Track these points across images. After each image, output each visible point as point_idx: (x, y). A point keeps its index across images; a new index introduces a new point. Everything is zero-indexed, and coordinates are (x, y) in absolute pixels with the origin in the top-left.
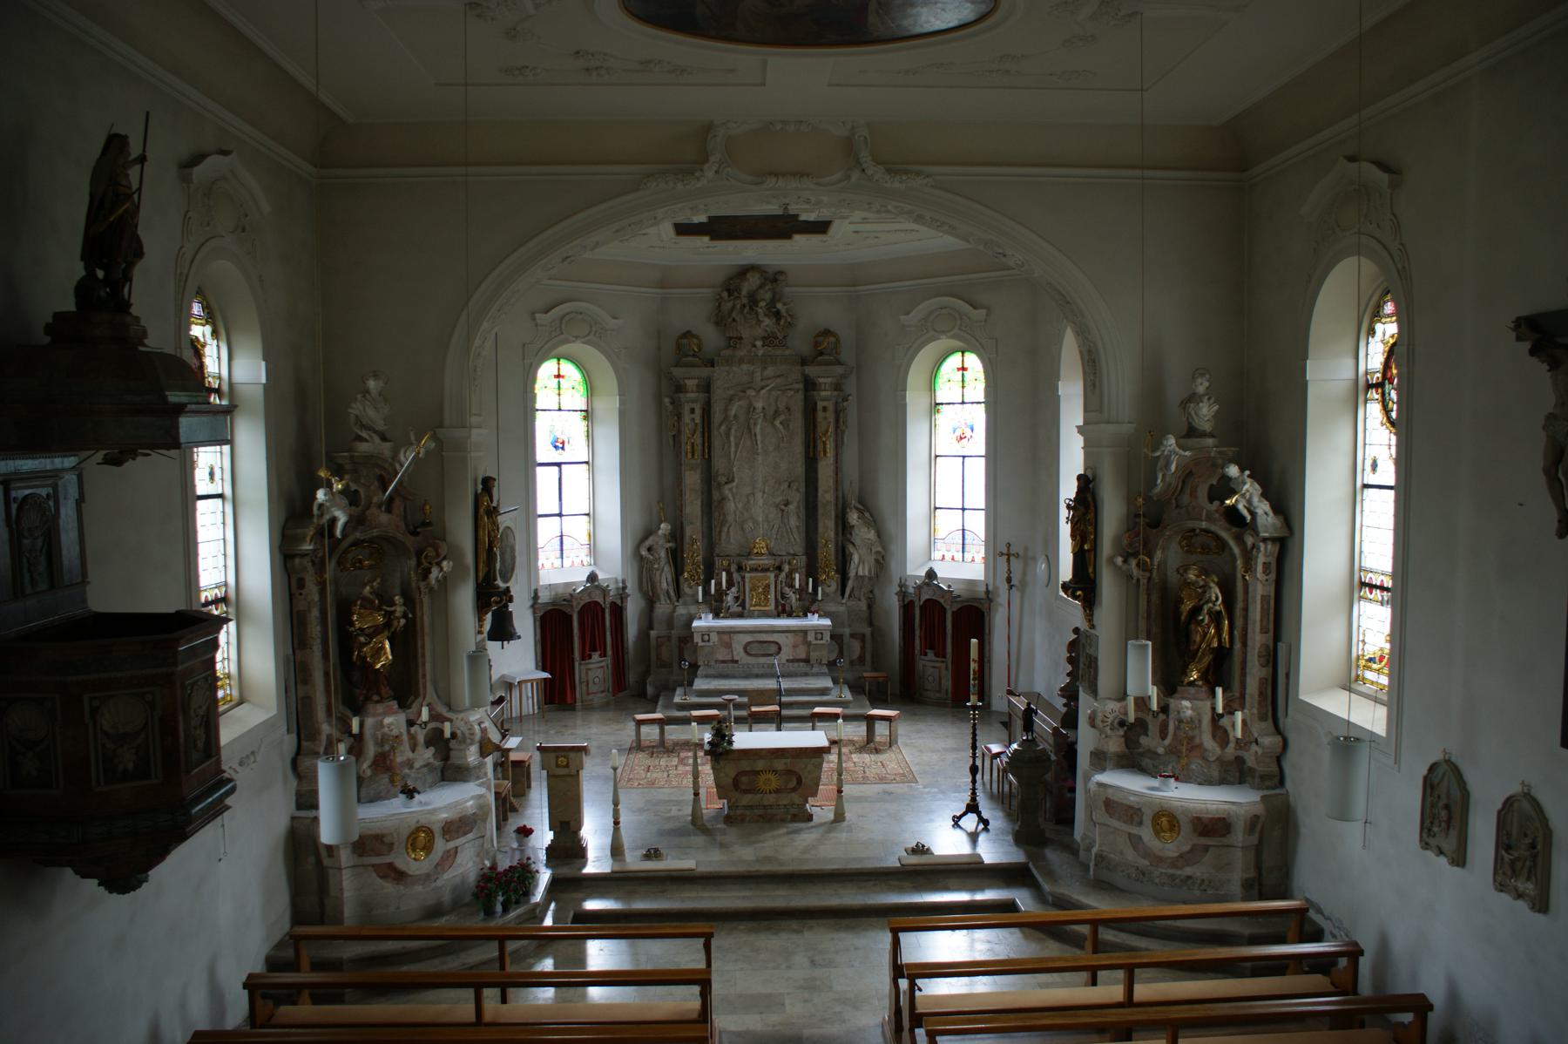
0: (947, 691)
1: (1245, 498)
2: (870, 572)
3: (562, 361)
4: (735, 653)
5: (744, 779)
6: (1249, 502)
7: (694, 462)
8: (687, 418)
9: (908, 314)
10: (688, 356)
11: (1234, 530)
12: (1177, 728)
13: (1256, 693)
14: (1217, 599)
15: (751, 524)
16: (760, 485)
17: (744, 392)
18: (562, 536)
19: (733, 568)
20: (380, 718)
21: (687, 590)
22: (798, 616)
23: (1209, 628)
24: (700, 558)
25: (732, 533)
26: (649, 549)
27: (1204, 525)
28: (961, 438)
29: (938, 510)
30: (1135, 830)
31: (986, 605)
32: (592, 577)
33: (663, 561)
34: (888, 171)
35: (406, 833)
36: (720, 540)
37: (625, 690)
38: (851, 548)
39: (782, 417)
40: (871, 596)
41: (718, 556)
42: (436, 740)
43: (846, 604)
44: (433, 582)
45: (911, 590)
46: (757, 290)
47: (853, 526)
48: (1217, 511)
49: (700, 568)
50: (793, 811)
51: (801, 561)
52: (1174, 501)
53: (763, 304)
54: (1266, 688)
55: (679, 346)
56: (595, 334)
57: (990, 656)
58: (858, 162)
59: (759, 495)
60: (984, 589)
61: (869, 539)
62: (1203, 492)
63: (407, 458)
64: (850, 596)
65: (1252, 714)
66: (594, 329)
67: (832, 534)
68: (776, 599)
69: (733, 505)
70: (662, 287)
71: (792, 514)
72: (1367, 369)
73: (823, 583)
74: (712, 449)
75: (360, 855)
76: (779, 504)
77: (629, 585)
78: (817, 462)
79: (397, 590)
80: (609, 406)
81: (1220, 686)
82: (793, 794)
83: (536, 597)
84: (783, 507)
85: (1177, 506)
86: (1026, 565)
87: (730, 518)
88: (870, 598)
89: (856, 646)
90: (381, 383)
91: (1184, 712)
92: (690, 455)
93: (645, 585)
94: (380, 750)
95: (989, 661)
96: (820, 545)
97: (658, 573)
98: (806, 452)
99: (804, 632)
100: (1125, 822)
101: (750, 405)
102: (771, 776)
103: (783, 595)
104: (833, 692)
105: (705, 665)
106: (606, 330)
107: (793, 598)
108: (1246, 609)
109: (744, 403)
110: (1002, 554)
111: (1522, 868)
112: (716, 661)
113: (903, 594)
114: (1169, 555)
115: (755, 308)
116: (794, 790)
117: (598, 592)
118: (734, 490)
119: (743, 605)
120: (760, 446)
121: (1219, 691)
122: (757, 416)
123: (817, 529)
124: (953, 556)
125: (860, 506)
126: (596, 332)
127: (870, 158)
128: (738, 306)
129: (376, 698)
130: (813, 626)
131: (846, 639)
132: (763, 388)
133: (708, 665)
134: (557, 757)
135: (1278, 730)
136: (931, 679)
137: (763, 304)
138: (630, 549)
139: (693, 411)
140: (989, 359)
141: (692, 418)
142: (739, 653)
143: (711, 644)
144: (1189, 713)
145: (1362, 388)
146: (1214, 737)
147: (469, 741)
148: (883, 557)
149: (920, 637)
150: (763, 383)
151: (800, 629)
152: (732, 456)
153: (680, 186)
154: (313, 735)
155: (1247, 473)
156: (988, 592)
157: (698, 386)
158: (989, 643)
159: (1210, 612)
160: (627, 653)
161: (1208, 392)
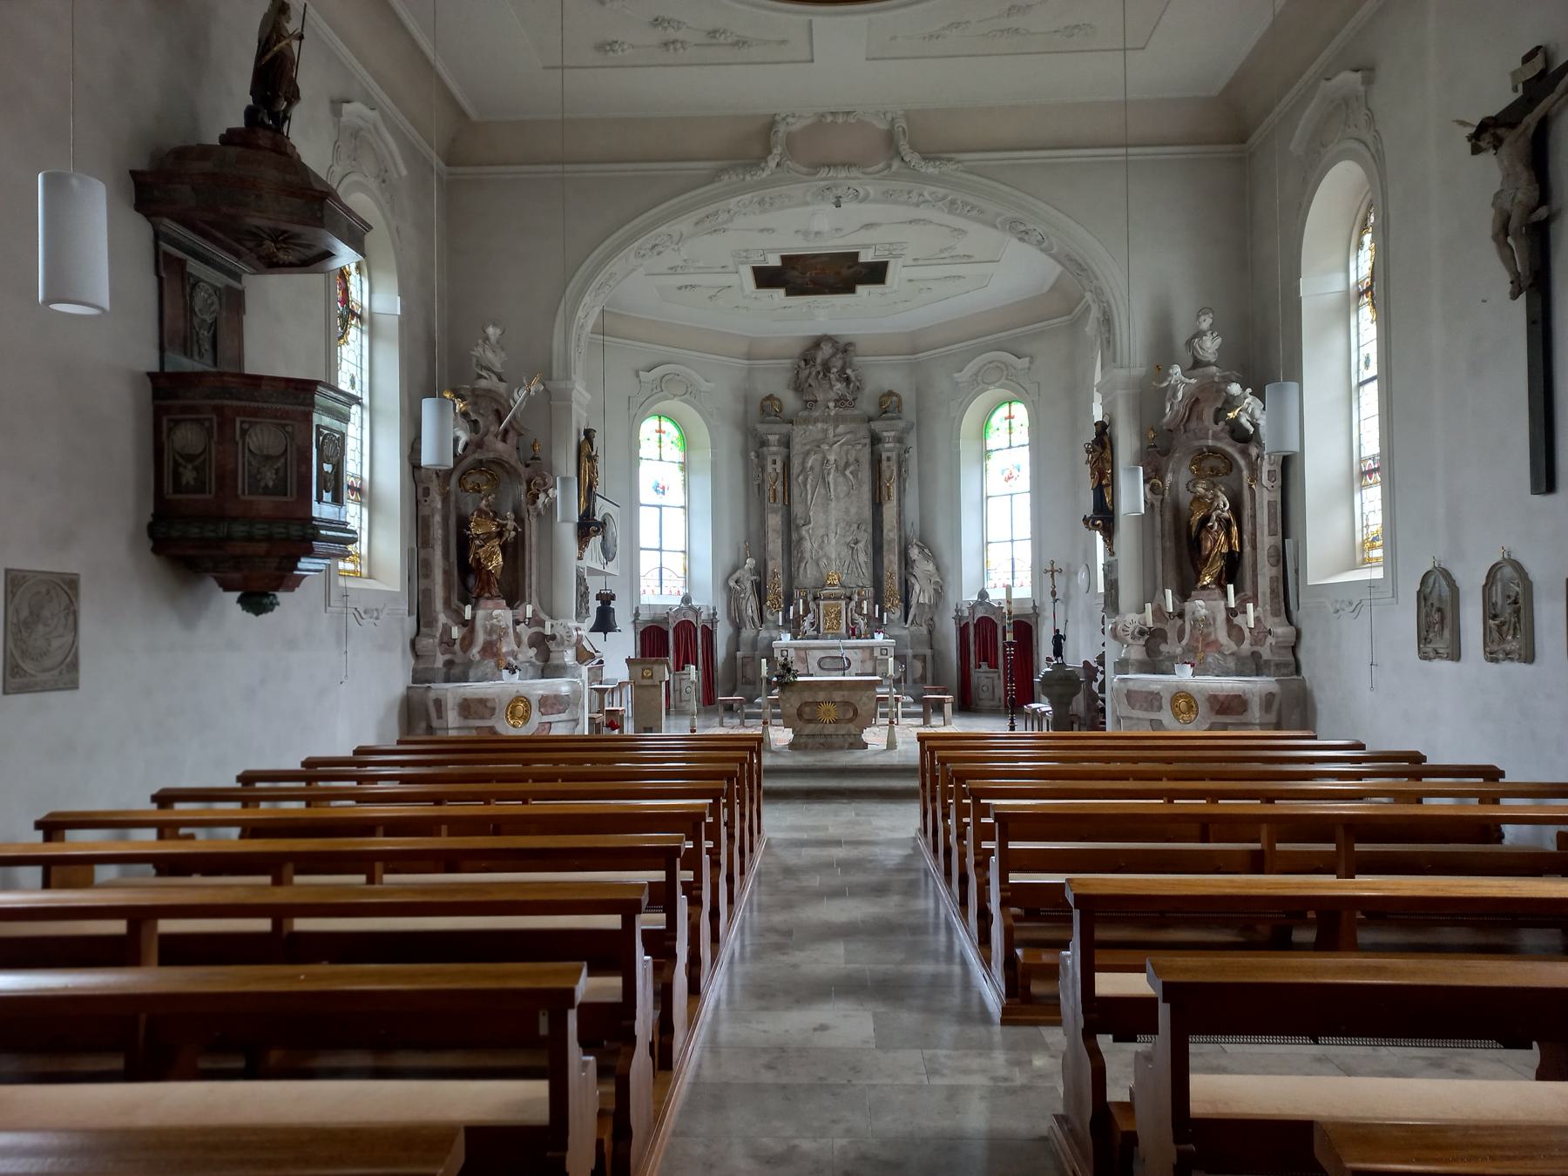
0: (1000, 699)
1: (1247, 413)
2: (930, 600)
5: (807, 709)
6: (1252, 415)
7: (775, 505)
8: (770, 468)
9: (960, 371)
10: (770, 415)
11: (1240, 445)
12: (1193, 627)
13: (1268, 591)
14: (1225, 506)
16: (833, 527)
17: (819, 447)
18: (661, 568)
19: (810, 598)
20: (489, 611)
21: (769, 617)
23: (1219, 535)
27: (1210, 443)
28: (1009, 478)
30: (1154, 716)
31: (1034, 620)
32: (686, 599)
33: (749, 591)
34: (924, 159)
35: (506, 701)
36: (798, 574)
39: (852, 468)
41: (797, 588)
42: (542, 643)
43: (908, 628)
44: (540, 506)
45: (966, 614)
46: (829, 358)
48: (1222, 430)
50: (850, 740)
51: (869, 592)
52: (1182, 427)
53: (834, 370)
54: (1277, 587)
55: (763, 409)
56: (690, 394)
57: (1038, 664)
58: (898, 153)
59: (832, 535)
62: (1208, 415)
63: (520, 396)
65: (1265, 611)
66: (690, 390)
67: (896, 568)
69: (809, 544)
70: (748, 359)
72: (1357, 280)
73: (888, 610)
75: (466, 718)
78: (882, 506)
79: (510, 505)
80: (704, 456)
81: (1231, 583)
83: (637, 615)
84: (853, 545)
85: (1185, 431)
86: (1069, 579)
87: (807, 555)
89: (918, 665)
90: (498, 332)
91: (1199, 611)
94: (488, 638)
96: (885, 578)
99: (871, 648)
100: (1145, 710)
101: (824, 457)
102: (830, 706)
106: (700, 392)
107: (862, 623)
108: (1254, 516)
109: (819, 456)
111: (1509, 629)
113: (958, 618)
114: (1179, 476)
116: (851, 720)
117: (691, 613)
119: (818, 630)
121: (1231, 588)
125: (920, 544)
126: (691, 392)
127: (908, 146)
128: (814, 373)
129: (487, 595)
131: (909, 660)
134: (643, 670)
135: (1290, 622)
137: (834, 370)
138: (720, 582)
139: (774, 462)
140: (1033, 401)
141: (774, 468)
144: (1203, 612)
145: (1349, 302)
146: (1229, 636)
147: (566, 643)
150: (836, 439)
152: (809, 503)
153: (748, 178)
154: (431, 623)
155: (1249, 390)
156: (1034, 607)
157: (779, 440)
159: (1219, 519)
161: (1212, 328)
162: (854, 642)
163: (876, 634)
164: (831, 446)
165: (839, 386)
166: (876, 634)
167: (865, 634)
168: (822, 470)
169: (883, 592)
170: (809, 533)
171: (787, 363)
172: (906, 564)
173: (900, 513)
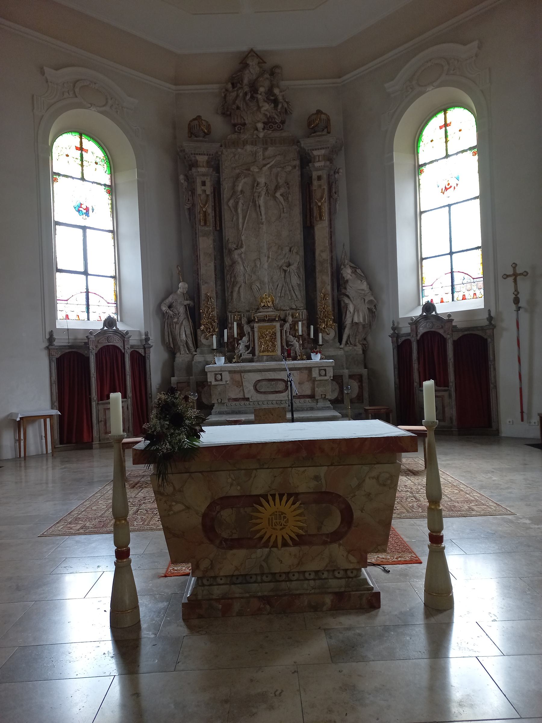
0: (451, 419)
2: (364, 320)
5: (227, 515)
7: (207, 229)
8: (199, 190)
15: (258, 285)
17: (248, 169)
19: (244, 321)
21: (204, 341)
22: (302, 359)
24: (215, 313)
25: (242, 294)
26: (170, 307)
28: (446, 189)
29: (424, 261)
36: (232, 299)
38: (347, 300)
39: (282, 190)
40: (365, 343)
41: (231, 312)
47: (347, 281)
49: (215, 322)
50: (335, 584)
51: (303, 313)
57: (496, 382)
60: (487, 316)
61: (363, 290)
64: (347, 343)
67: (329, 288)
68: (282, 346)
69: (242, 268)
70: (176, 84)
73: (323, 331)
77: (152, 337)
78: (314, 229)
82: (335, 546)
83: (51, 340)
84: (285, 268)
87: (240, 279)
88: (363, 344)
89: (355, 385)
92: (202, 223)
93: (167, 337)
95: (495, 387)
96: (319, 299)
97: (177, 326)
99: (309, 369)
101: (254, 180)
103: (287, 342)
107: (297, 345)
110: (508, 276)
112: (229, 399)
113: (396, 335)
115: (255, 95)
118: (243, 255)
119: (253, 353)
122: (260, 190)
123: (315, 283)
124: (442, 299)
128: (241, 95)
130: (317, 363)
131: (346, 379)
132: (265, 165)
133: (221, 403)
139: (204, 184)
142: (249, 391)
148: (375, 306)
149: (418, 370)
150: (265, 162)
152: (240, 226)
156: (490, 318)
157: (208, 162)
158: (495, 369)
160: (151, 398)
162: (290, 363)
164: (261, 169)
165: (266, 107)
167: (301, 356)
172: (339, 286)
173: (331, 234)
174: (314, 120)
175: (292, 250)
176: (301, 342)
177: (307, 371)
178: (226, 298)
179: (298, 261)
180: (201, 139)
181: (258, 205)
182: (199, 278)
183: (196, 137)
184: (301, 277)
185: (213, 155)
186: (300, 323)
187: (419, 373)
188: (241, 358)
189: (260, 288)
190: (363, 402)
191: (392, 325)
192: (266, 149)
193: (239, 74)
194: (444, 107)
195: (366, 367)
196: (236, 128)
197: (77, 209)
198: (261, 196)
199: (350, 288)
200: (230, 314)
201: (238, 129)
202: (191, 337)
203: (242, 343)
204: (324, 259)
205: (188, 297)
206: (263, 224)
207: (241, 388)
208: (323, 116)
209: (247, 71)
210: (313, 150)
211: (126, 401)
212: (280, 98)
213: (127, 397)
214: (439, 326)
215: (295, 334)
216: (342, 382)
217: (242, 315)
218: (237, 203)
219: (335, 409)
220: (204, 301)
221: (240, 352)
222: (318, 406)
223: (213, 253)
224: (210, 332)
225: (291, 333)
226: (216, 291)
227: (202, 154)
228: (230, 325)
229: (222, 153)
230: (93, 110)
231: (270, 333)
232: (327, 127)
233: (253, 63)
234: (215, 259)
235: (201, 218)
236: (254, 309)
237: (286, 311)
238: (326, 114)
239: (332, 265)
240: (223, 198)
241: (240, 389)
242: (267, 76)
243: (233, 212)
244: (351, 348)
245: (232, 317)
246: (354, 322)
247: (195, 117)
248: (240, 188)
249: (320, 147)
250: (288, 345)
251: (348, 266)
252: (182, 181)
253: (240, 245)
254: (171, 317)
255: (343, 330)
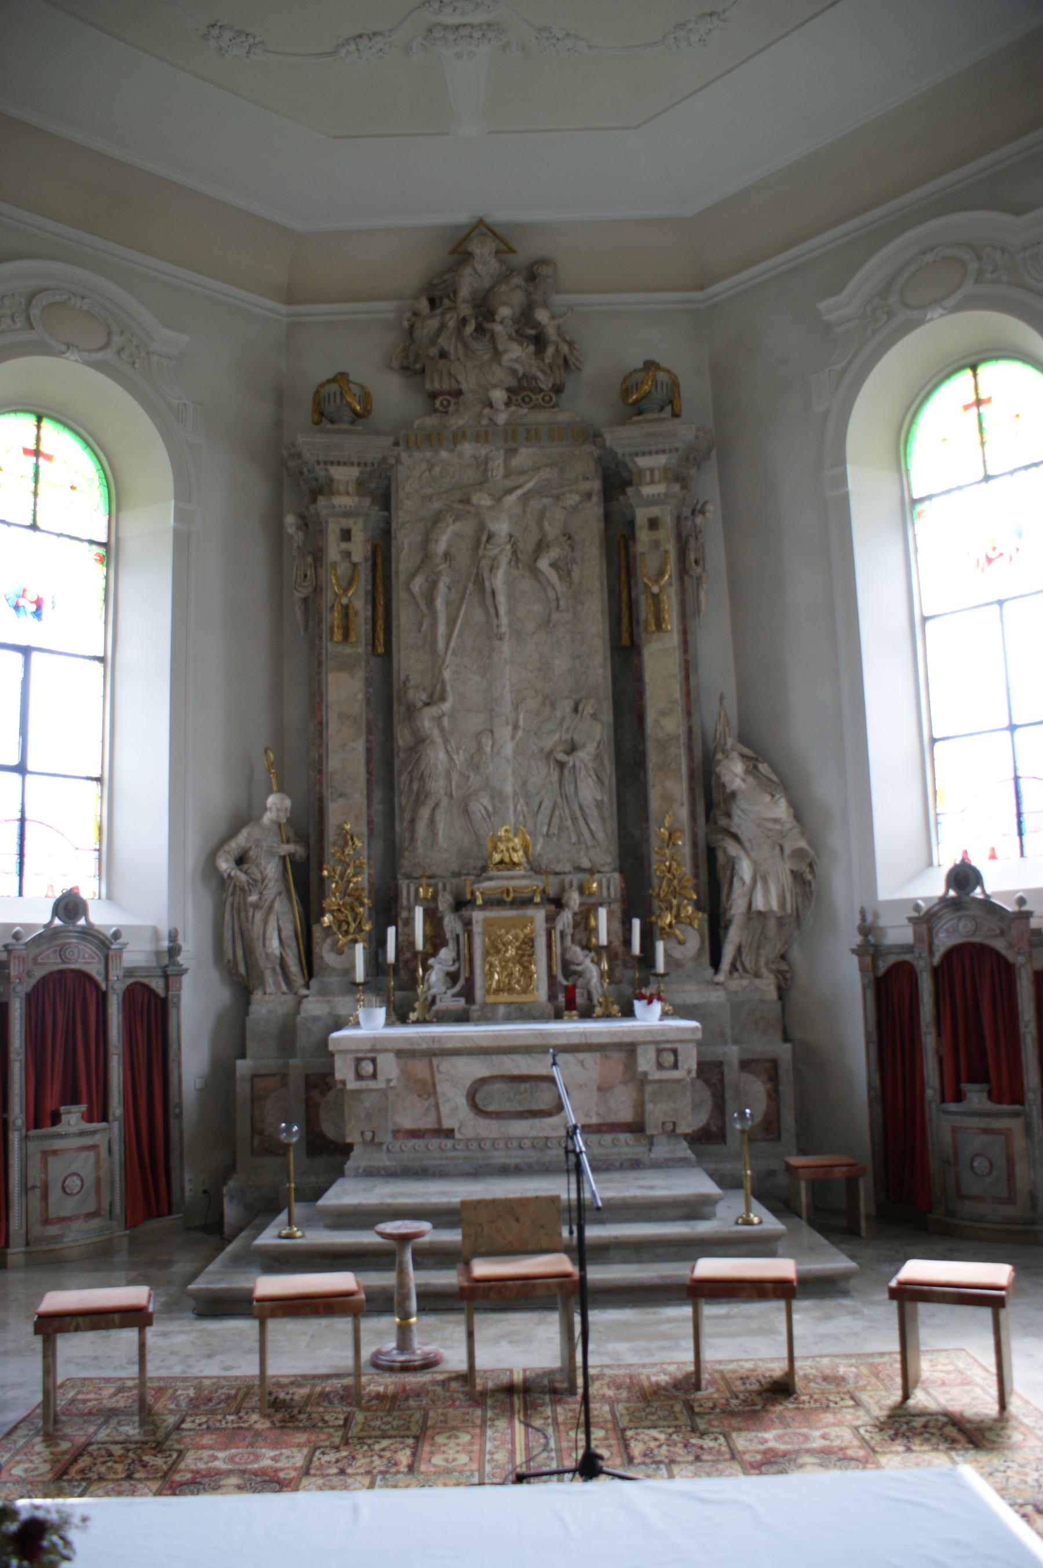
3: (46, 423)
4: (445, 1110)
7: (348, 650)
8: (334, 551)
9: (838, 291)
15: (486, 801)
17: (467, 501)
19: (444, 903)
22: (607, 1016)
26: (241, 860)
36: (413, 839)
37: (170, 1213)
38: (732, 849)
39: (554, 553)
40: (784, 967)
41: (408, 876)
47: (733, 795)
49: (362, 904)
59: (505, 732)
61: (776, 820)
64: (733, 967)
67: (684, 813)
68: (551, 977)
69: (442, 755)
70: (289, 302)
71: (583, 773)
73: (667, 934)
74: (394, 632)
76: (552, 751)
84: (561, 757)
87: (437, 786)
89: (757, 1087)
92: (338, 636)
93: (228, 945)
96: (655, 844)
97: (259, 916)
98: (611, 633)
99: (629, 1049)
101: (481, 527)
103: (566, 964)
104: (721, 1209)
105: (365, 1143)
109: (467, 527)
112: (396, 1133)
115: (487, 325)
118: (446, 721)
119: (468, 994)
120: (504, 620)
122: (497, 551)
128: (452, 324)
130: (650, 1031)
131: (732, 1074)
132: (509, 491)
133: (374, 1143)
136: (979, 1163)
138: (192, 858)
139: (346, 535)
143: (380, 1084)
150: (509, 483)
151: (616, 1040)
152: (441, 645)
157: (360, 483)
160: (180, 1116)
162: (571, 1028)
163: (639, 1006)
164: (499, 500)
165: (516, 353)
166: (639, 1006)
167: (605, 1005)
168: (476, 559)
169: (650, 885)
170: (442, 729)
171: (386, 309)
172: (709, 806)
173: (688, 669)
174: (637, 384)
175: (581, 708)
176: (605, 966)
177: (622, 1055)
178: (397, 837)
179: (598, 738)
180: (345, 426)
181: (488, 590)
182: (324, 780)
183: (332, 421)
184: (606, 782)
185: (373, 464)
186: (603, 913)
187: (940, 1060)
188: (435, 1008)
189: (490, 809)
190: (779, 1138)
191: (858, 921)
192: (511, 452)
193: (447, 277)
194: (971, 360)
195: (786, 1039)
196: (438, 403)
197: (13, 603)
198: (498, 567)
199: (743, 815)
200: (406, 881)
201: (442, 404)
202: (294, 944)
203: (437, 967)
204: (668, 735)
205: (291, 834)
206: (501, 639)
207: (432, 1101)
208: (661, 376)
209: (468, 270)
210: (637, 455)
211: (104, 1130)
212: (551, 332)
213: (111, 1118)
214: (994, 930)
215: (589, 940)
216: (722, 1080)
217: (440, 886)
218: (433, 585)
219: (701, 1160)
220: (334, 844)
221: (433, 991)
222: (653, 1156)
223: (364, 717)
224: (347, 933)
225: (577, 937)
226: (369, 816)
227: (345, 464)
228: (404, 914)
229: (398, 460)
230: (72, 358)
231: (516, 938)
232: (671, 402)
233: (483, 250)
234: (369, 731)
235: (336, 622)
236: (475, 868)
237: (562, 877)
238: (669, 372)
239: (690, 749)
240: (397, 572)
241: (427, 1104)
242: (517, 280)
243: (423, 606)
244: (745, 982)
245: (412, 889)
246: (754, 908)
247: (331, 376)
248: (441, 546)
249: (653, 448)
250: (568, 972)
251: (734, 755)
252: (291, 530)
253: (437, 694)
254: (242, 889)
255: (722, 932)
